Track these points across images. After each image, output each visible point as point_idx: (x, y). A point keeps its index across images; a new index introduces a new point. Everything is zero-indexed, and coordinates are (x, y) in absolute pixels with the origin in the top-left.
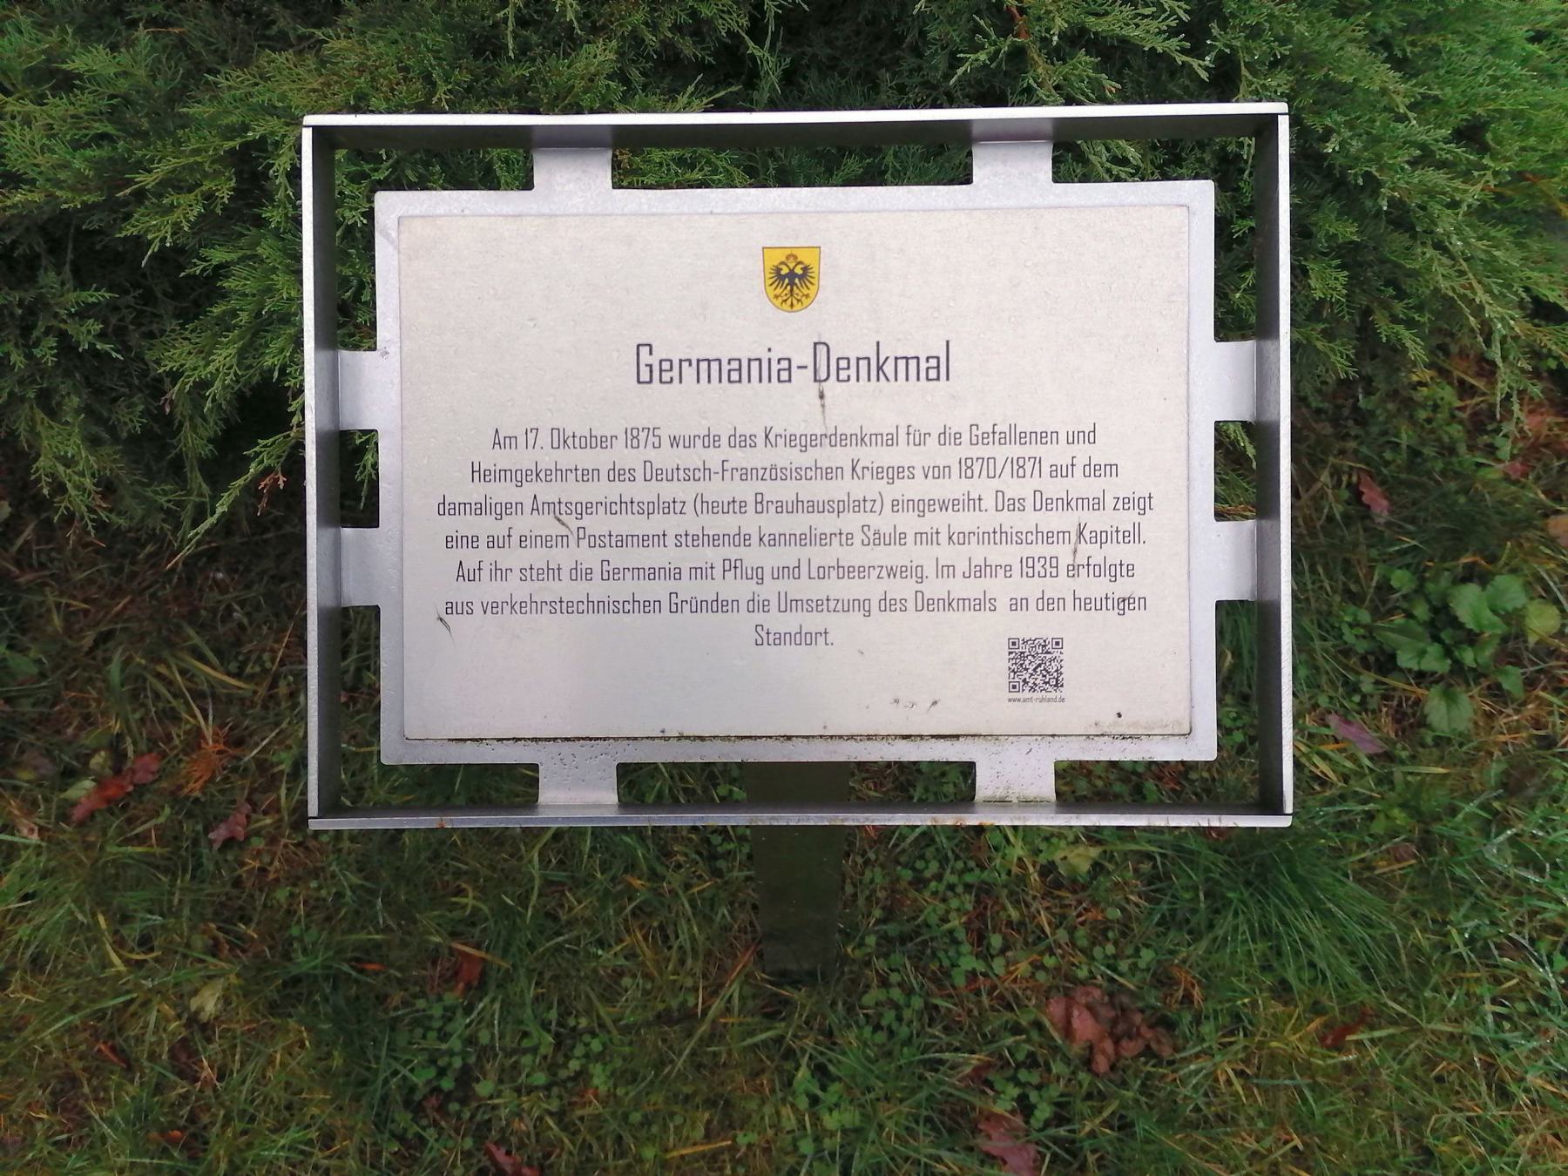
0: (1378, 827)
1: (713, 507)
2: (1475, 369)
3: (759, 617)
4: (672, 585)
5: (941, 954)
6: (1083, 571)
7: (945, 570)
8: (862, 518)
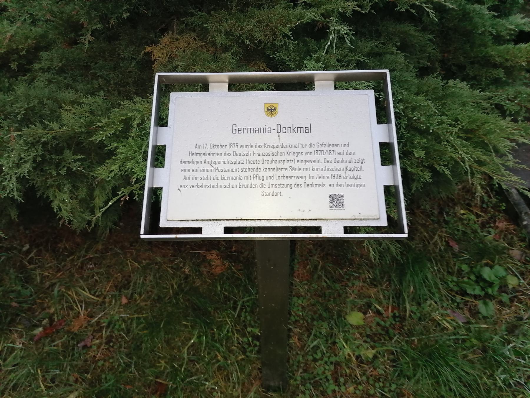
0: (468, 344)
1: (251, 162)
2: (480, 210)
3: (263, 189)
4: (240, 181)
5: (323, 385)
6: (348, 177)
7: (312, 177)
8: (290, 165)
